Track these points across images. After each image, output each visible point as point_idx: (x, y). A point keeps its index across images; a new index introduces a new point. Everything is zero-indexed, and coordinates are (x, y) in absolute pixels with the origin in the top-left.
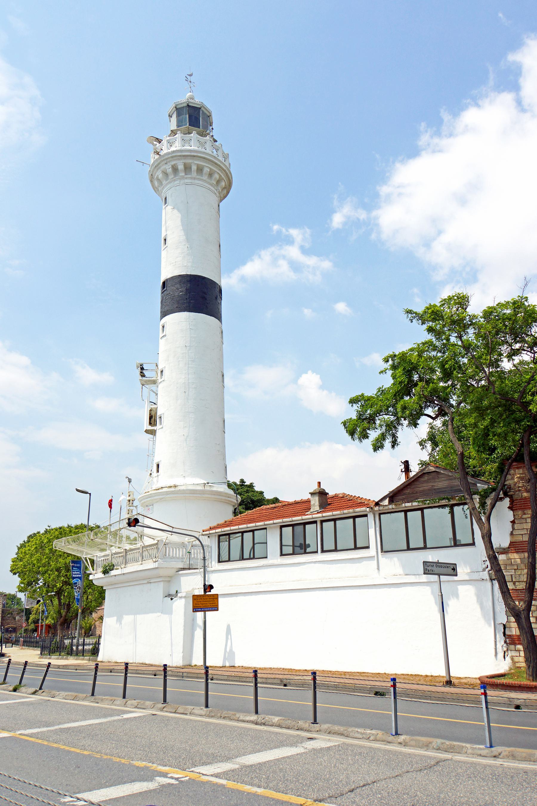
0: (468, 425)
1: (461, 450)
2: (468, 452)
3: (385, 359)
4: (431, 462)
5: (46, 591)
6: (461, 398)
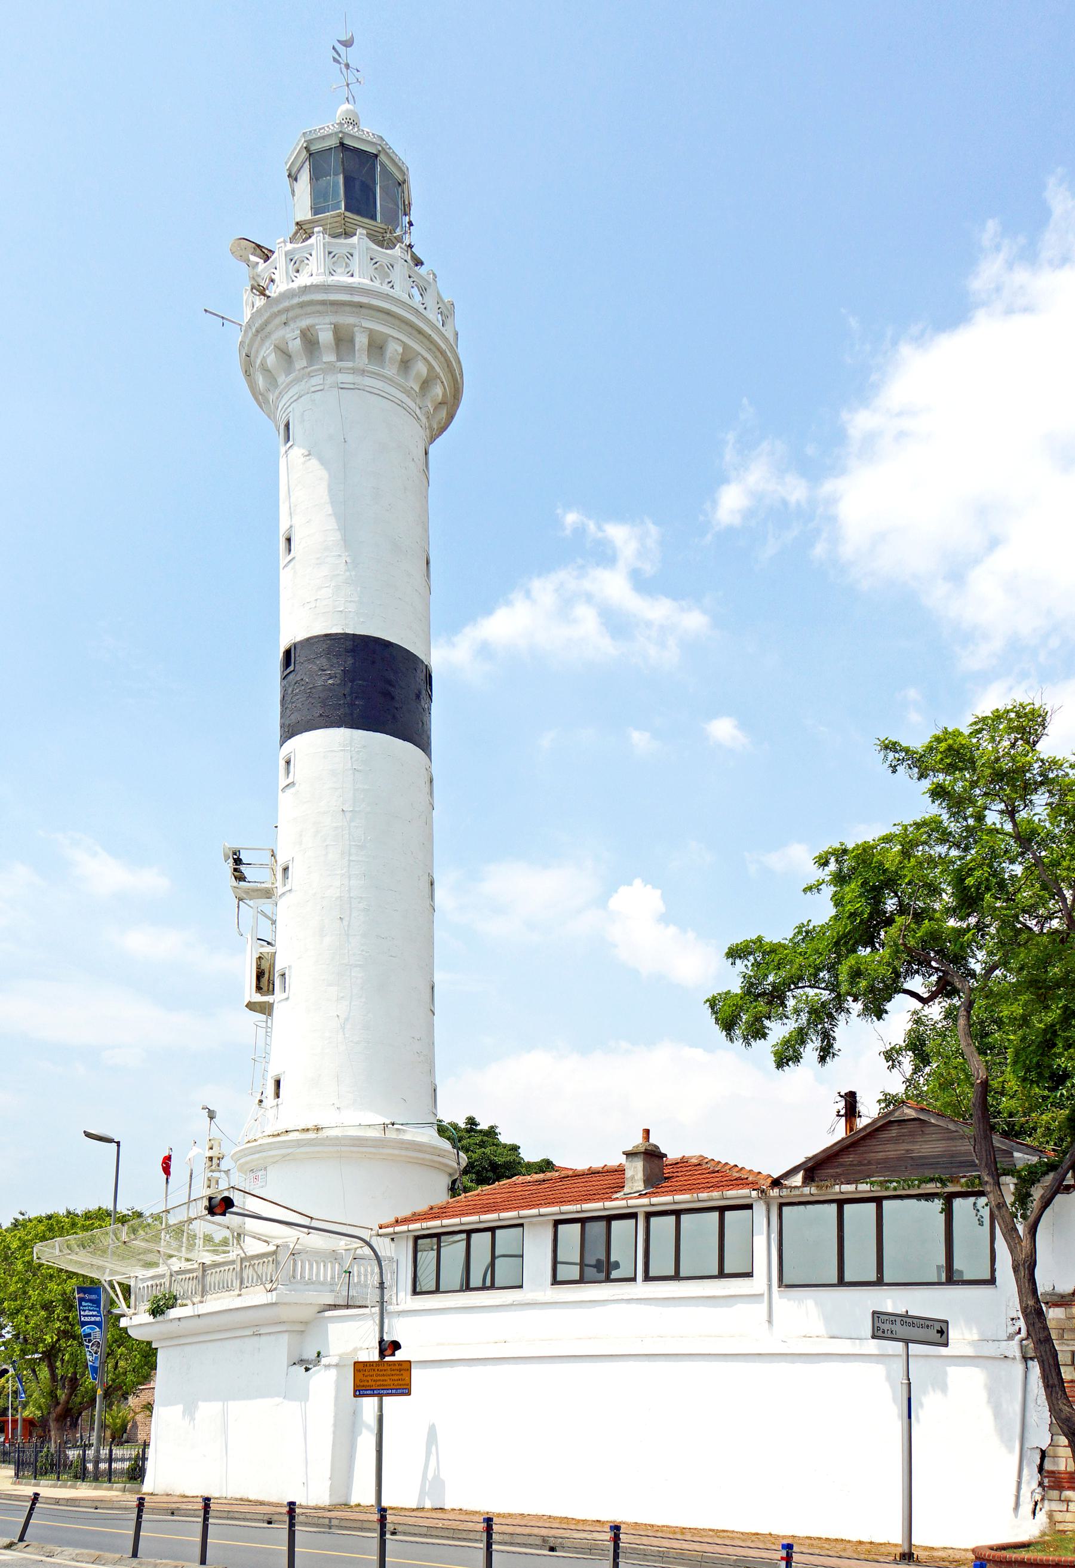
0: (1006, 1021)
1: (983, 1074)
2: (1001, 1079)
3: (820, 857)
4: (908, 1097)
5: (21, 1350)
6: (996, 958)
